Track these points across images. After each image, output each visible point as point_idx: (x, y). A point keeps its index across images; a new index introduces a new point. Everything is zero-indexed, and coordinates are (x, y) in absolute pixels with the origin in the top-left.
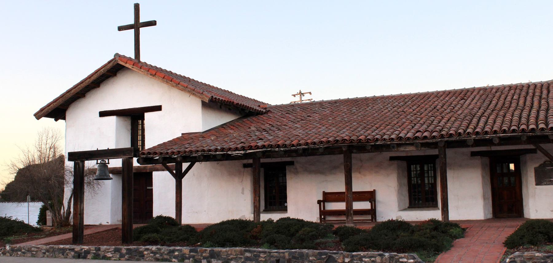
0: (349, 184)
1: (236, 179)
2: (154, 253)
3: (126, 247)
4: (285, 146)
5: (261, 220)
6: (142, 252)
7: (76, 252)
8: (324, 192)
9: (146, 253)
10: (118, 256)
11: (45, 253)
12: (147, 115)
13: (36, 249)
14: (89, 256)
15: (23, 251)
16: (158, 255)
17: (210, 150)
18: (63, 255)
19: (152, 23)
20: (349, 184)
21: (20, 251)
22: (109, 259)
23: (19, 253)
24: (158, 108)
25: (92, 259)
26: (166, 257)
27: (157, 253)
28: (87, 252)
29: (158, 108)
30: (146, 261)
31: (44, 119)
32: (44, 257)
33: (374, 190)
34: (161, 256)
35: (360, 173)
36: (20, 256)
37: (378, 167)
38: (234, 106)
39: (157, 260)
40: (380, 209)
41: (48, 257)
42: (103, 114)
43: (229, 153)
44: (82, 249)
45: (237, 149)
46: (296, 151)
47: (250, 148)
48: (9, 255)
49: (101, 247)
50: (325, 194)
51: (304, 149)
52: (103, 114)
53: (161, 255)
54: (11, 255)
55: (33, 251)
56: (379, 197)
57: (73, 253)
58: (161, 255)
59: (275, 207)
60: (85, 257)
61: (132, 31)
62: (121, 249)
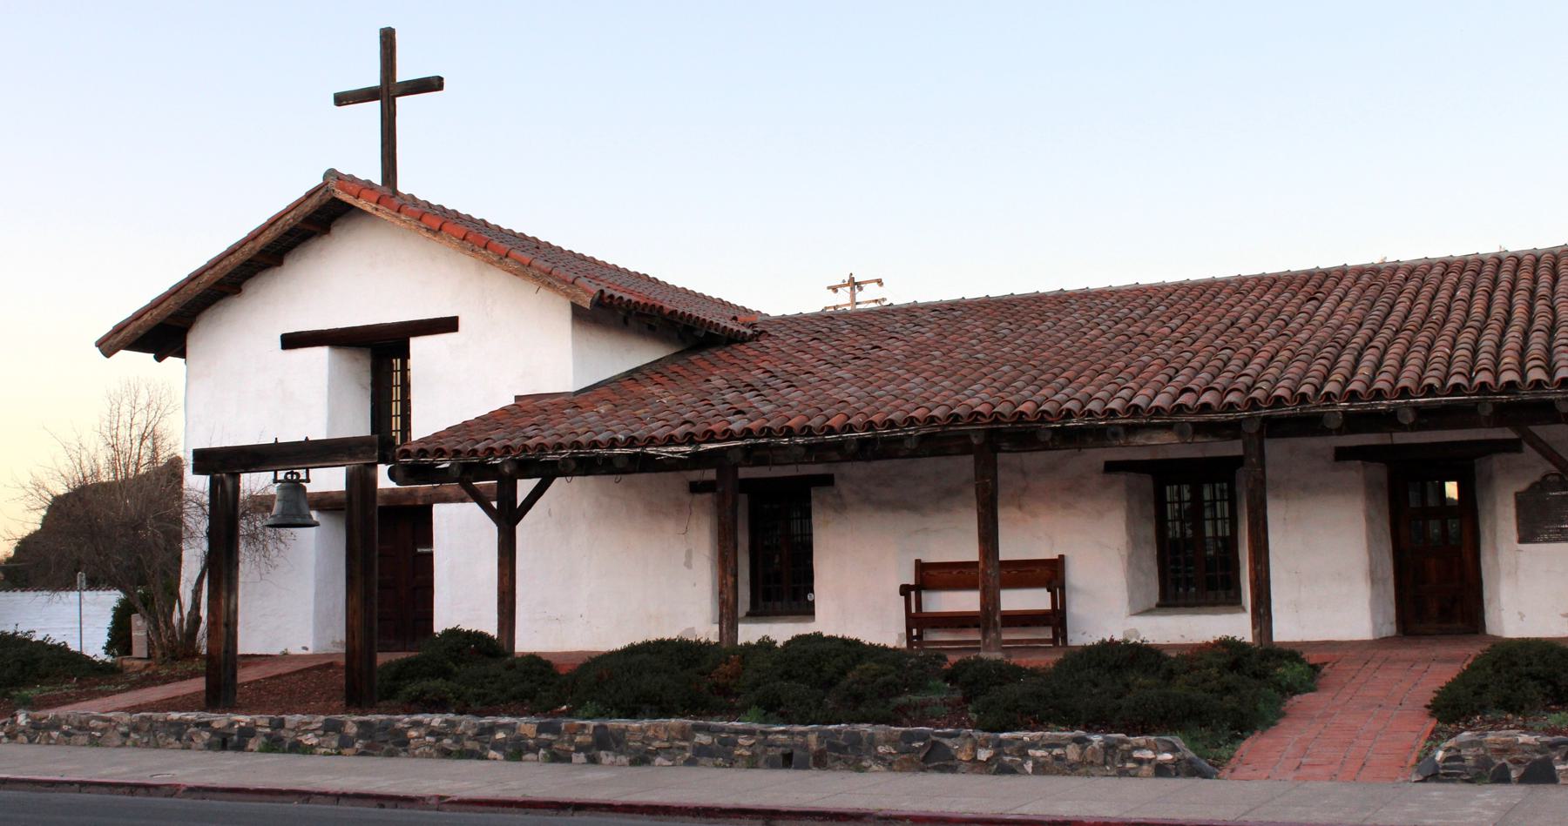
0: (989, 538)
1: (670, 526)
2: (437, 734)
3: (356, 718)
4: (807, 431)
5: (741, 641)
6: (403, 732)
7: (215, 732)
8: (918, 562)
9: (413, 733)
10: (335, 744)
11: (126, 735)
12: (417, 345)
14: (253, 744)
15: (65, 727)
16: (447, 741)
17: (595, 444)
18: (179, 739)
19: (432, 85)
20: (989, 538)
21: (58, 728)
22: (309, 750)
23: (55, 734)
24: (449, 325)
25: (261, 751)
26: (469, 745)
27: (446, 735)
28: (248, 732)
29: (449, 325)
30: (415, 756)
32: (124, 745)
33: (1062, 557)
34: (456, 742)
35: (1020, 507)
37: (1072, 491)
38: (664, 317)
39: (446, 754)
40: (1077, 609)
41: (135, 745)
42: (291, 341)
43: (650, 450)
44: (232, 724)
45: (671, 440)
46: (839, 446)
47: (710, 436)
48: (25, 739)
49: (287, 717)
50: (921, 567)
51: (861, 440)
52: (291, 341)
53: (458, 739)
54: (31, 741)
55: (94, 729)
56: (1075, 575)
57: (206, 735)
58: (458, 739)
60: (240, 747)
61: (375, 107)
62: (343, 724)
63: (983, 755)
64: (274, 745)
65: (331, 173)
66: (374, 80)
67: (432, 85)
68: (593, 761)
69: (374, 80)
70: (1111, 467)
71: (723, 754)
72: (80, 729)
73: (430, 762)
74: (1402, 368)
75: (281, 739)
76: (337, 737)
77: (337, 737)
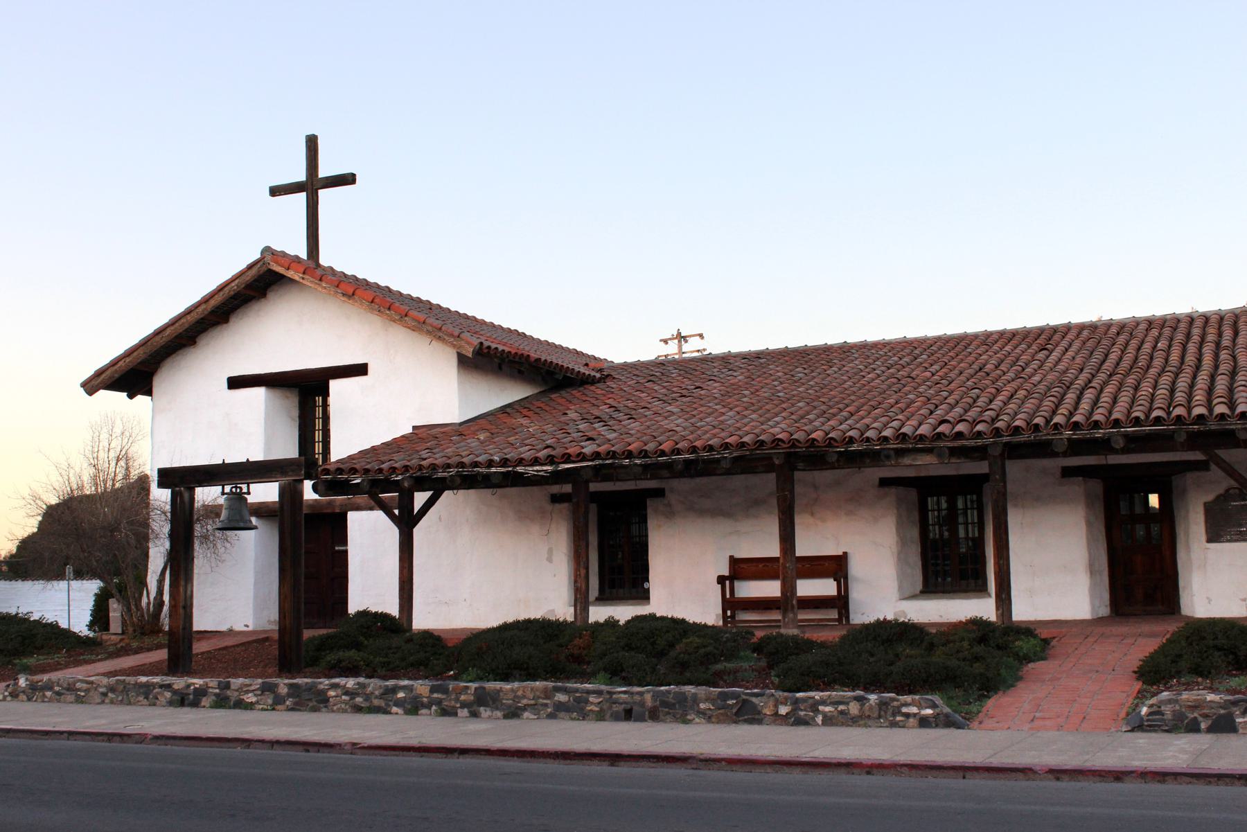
0: (787, 539)
1: (535, 529)
3: (287, 681)
4: (644, 454)
5: (592, 620)
6: (324, 692)
7: (175, 692)
8: (731, 557)
9: (332, 693)
11: (105, 695)
12: (335, 385)
13: (85, 686)
14: (205, 701)
15: (57, 689)
16: (359, 700)
17: (476, 464)
18: (147, 698)
19: (347, 180)
20: (787, 539)
21: (51, 689)
22: (249, 707)
23: (48, 694)
24: (360, 370)
25: (211, 707)
26: (376, 702)
27: (358, 695)
29: (360, 370)
30: (333, 711)
31: (103, 394)
32: (103, 702)
33: (845, 554)
34: (366, 700)
35: (812, 514)
36: (51, 700)
37: (854, 502)
38: (530, 364)
39: (358, 709)
40: (857, 594)
41: (112, 702)
42: (236, 383)
43: (520, 469)
44: (188, 686)
45: (536, 461)
48: (25, 697)
50: (734, 562)
51: (686, 461)
52: (236, 383)
53: (368, 697)
54: (29, 699)
55: (79, 690)
56: (856, 568)
57: (168, 695)
58: (368, 697)
59: (621, 591)
60: (195, 704)
61: (302, 196)
62: (276, 685)
63: (783, 710)
64: (222, 702)
65: (267, 250)
66: (301, 176)
67: (347, 180)
68: (474, 715)
69: (301, 176)
70: (885, 483)
71: (577, 709)
72: (68, 690)
73: (345, 716)
74: (1115, 404)
75: (227, 698)
76: (272, 696)
77: (272, 696)
